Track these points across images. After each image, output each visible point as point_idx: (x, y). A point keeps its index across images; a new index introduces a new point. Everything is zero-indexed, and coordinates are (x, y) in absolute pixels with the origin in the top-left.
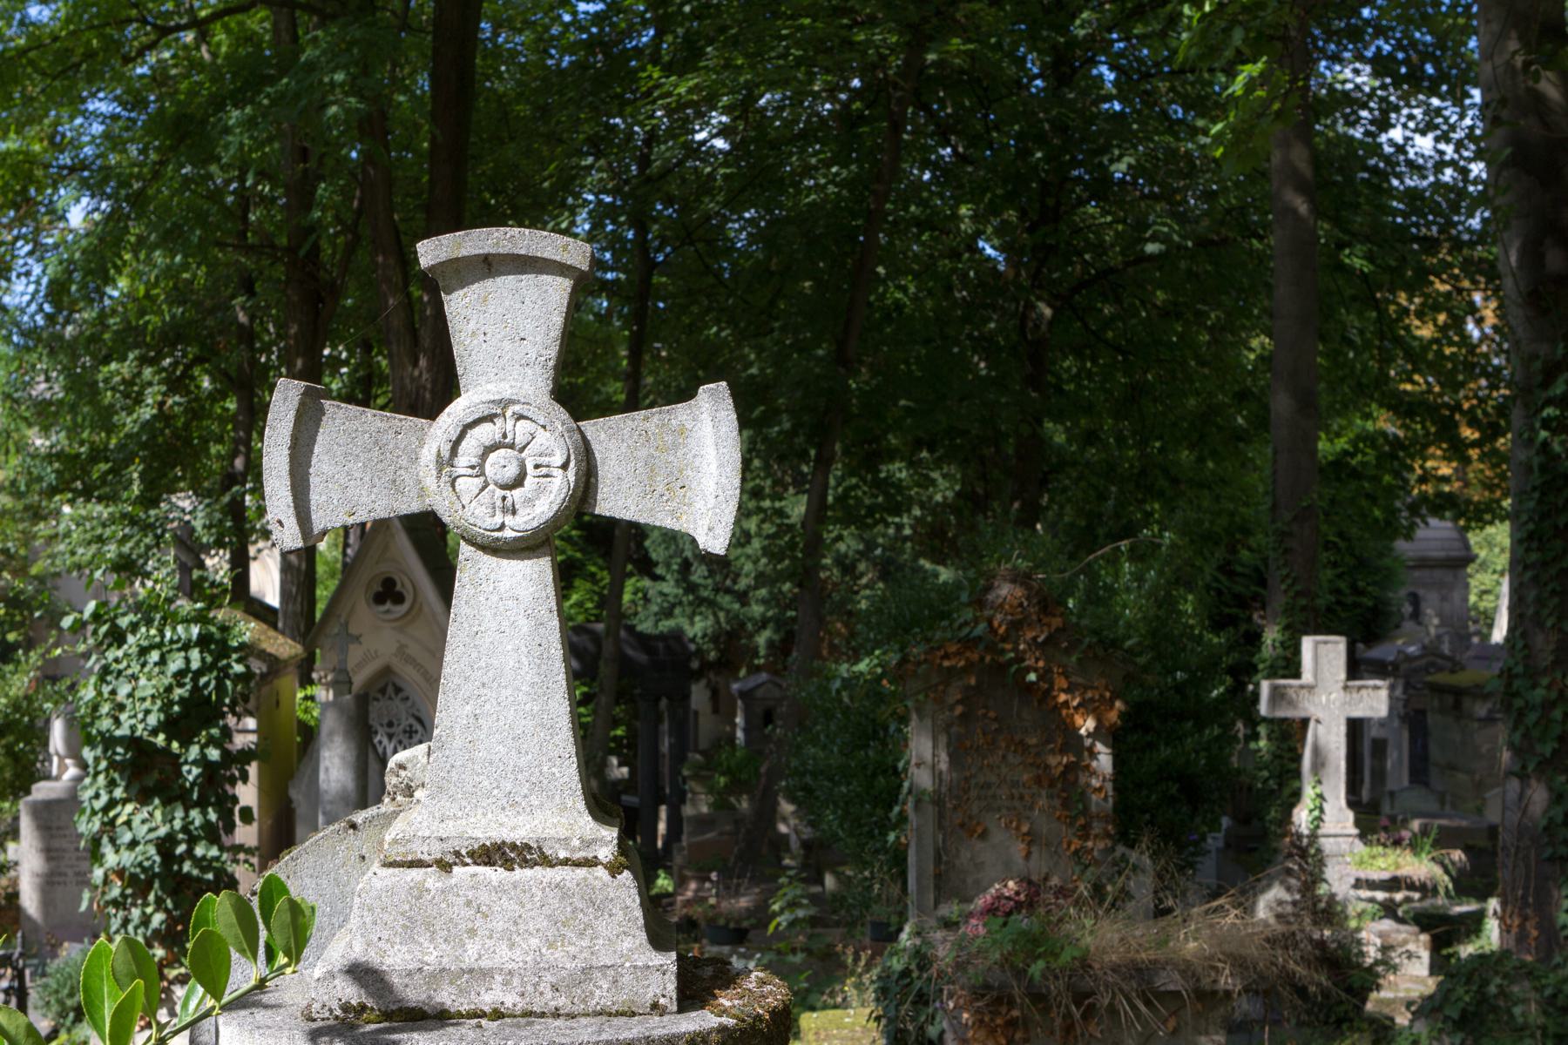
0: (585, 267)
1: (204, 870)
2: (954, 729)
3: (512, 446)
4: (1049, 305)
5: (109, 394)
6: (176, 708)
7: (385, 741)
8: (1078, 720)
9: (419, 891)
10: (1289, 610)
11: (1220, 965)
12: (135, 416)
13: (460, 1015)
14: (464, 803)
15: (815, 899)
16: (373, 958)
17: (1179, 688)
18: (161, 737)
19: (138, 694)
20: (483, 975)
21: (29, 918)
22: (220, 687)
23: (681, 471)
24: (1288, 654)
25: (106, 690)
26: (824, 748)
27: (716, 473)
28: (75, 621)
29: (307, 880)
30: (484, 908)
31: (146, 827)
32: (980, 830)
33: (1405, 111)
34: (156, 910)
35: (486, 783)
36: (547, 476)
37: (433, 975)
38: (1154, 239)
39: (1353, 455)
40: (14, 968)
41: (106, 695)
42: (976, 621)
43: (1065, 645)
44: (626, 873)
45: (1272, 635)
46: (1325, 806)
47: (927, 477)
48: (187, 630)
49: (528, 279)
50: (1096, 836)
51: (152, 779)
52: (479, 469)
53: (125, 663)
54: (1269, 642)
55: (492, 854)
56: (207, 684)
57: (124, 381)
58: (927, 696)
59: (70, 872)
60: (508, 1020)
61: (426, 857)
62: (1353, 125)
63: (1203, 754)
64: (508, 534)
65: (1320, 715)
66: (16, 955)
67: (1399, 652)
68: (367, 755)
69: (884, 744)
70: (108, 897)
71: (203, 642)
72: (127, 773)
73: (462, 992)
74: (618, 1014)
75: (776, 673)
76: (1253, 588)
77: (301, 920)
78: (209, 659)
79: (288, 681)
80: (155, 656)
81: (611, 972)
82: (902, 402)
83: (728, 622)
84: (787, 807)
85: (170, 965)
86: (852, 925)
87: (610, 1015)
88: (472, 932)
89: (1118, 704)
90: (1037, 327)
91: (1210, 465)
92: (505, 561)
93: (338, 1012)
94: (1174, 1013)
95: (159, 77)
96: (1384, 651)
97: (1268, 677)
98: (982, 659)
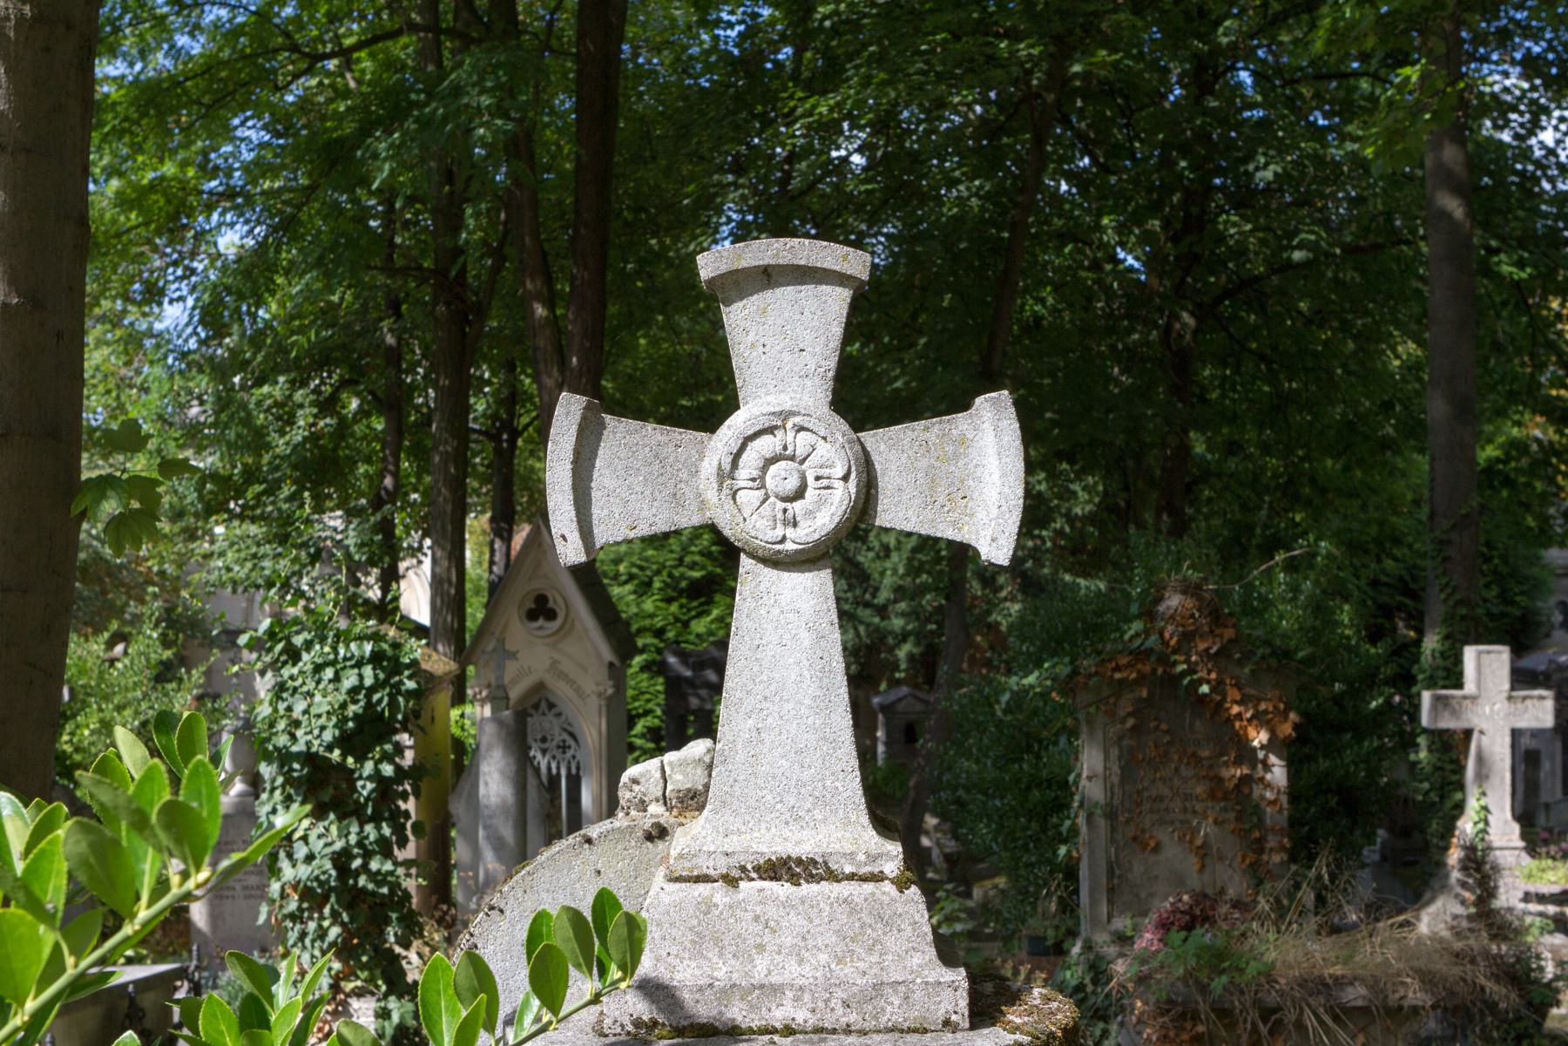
0: (865, 277)
1: (379, 884)
2: (1125, 742)
3: (792, 458)
4: (1192, 314)
5: (262, 416)
6: (351, 724)
7: (539, 756)
8: (1252, 732)
9: (707, 906)
10: (1448, 620)
11: (1409, 980)
12: (287, 437)
13: (751, 1031)
14: (747, 818)
15: (971, 913)
16: (663, 974)
17: (1338, 700)
18: (337, 753)
19: (313, 711)
20: (773, 991)
21: (199, 931)
22: (393, 704)
23: (962, 482)
24: (1448, 663)
25: (282, 706)
26: (977, 761)
27: (998, 483)
28: (251, 638)
29: (544, 895)
30: (772, 924)
31: (322, 842)
32: (1152, 844)
33: (1556, 114)
34: (332, 924)
35: (769, 797)
36: (828, 488)
37: (724, 991)
38: (1299, 247)
39: (1505, 462)
40: (191, 981)
41: (282, 712)
42: (1147, 632)
43: (1237, 656)
44: (914, 888)
45: (1431, 643)
46: (1490, 818)
47: (1068, 490)
48: (360, 647)
49: (808, 290)
50: (1271, 850)
51: (327, 795)
52: (759, 481)
53: (300, 681)
54: (1428, 652)
55: (777, 869)
56: (380, 701)
57: (276, 404)
58: (1098, 708)
59: (238, 886)
60: (801, 1037)
61: (711, 872)
62: (1501, 128)
63: (1362, 766)
64: (790, 546)
65: (1484, 726)
66: (192, 968)
67: (1551, 661)
68: (525, 770)
69: (1039, 757)
70: (285, 911)
71: (376, 659)
72: (304, 788)
73: (753, 1008)
74: (910, 1030)
75: (916, 686)
76: (1399, 598)
77: (637, 933)
78: (382, 676)
79: (443, 697)
80: (329, 673)
81: (902, 988)
82: (1048, 415)
83: (868, 636)
84: (931, 821)
85: (347, 978)
86: (1007, 939)
87: (902, 1031)
88: (761, 948)
89: (1293, 716)
90: (1181, 337)
91: (1359, 473)
92: (786, 574)
93: (630, 1028)
94: (1362, 1030)
95: (304, 103)
96: (1536, 661)
97: (1428, 688)
98: (1154, 671)
